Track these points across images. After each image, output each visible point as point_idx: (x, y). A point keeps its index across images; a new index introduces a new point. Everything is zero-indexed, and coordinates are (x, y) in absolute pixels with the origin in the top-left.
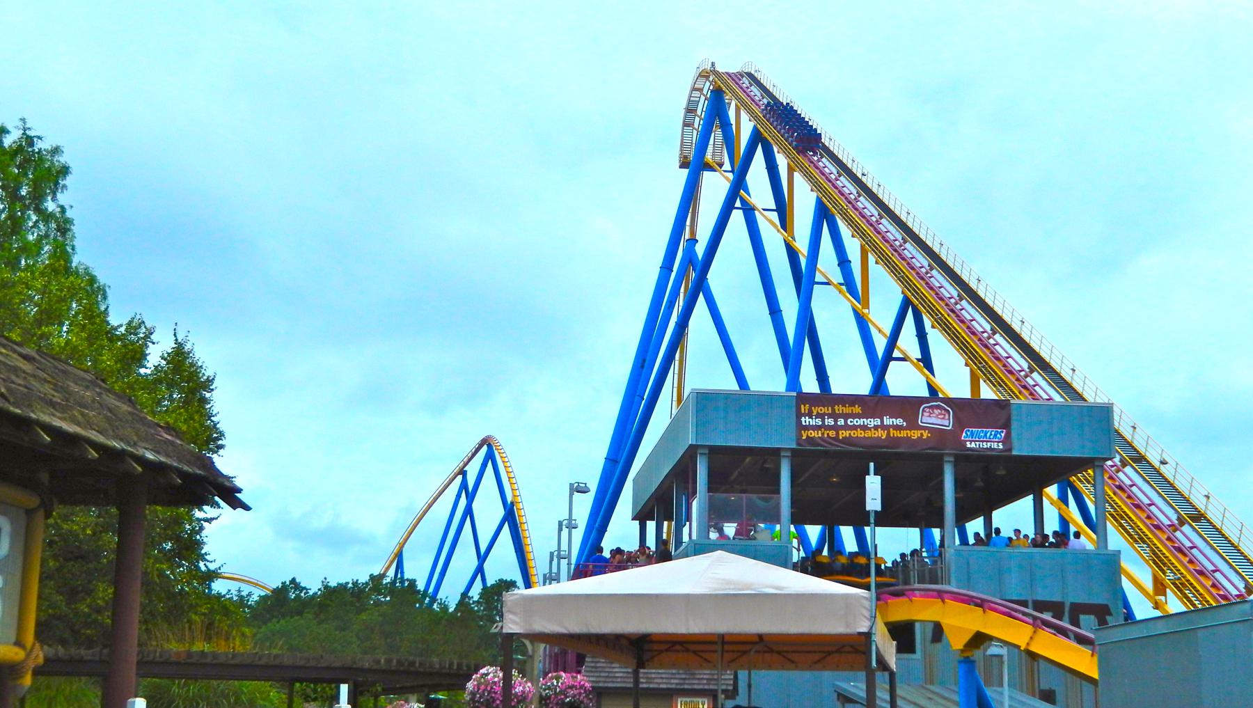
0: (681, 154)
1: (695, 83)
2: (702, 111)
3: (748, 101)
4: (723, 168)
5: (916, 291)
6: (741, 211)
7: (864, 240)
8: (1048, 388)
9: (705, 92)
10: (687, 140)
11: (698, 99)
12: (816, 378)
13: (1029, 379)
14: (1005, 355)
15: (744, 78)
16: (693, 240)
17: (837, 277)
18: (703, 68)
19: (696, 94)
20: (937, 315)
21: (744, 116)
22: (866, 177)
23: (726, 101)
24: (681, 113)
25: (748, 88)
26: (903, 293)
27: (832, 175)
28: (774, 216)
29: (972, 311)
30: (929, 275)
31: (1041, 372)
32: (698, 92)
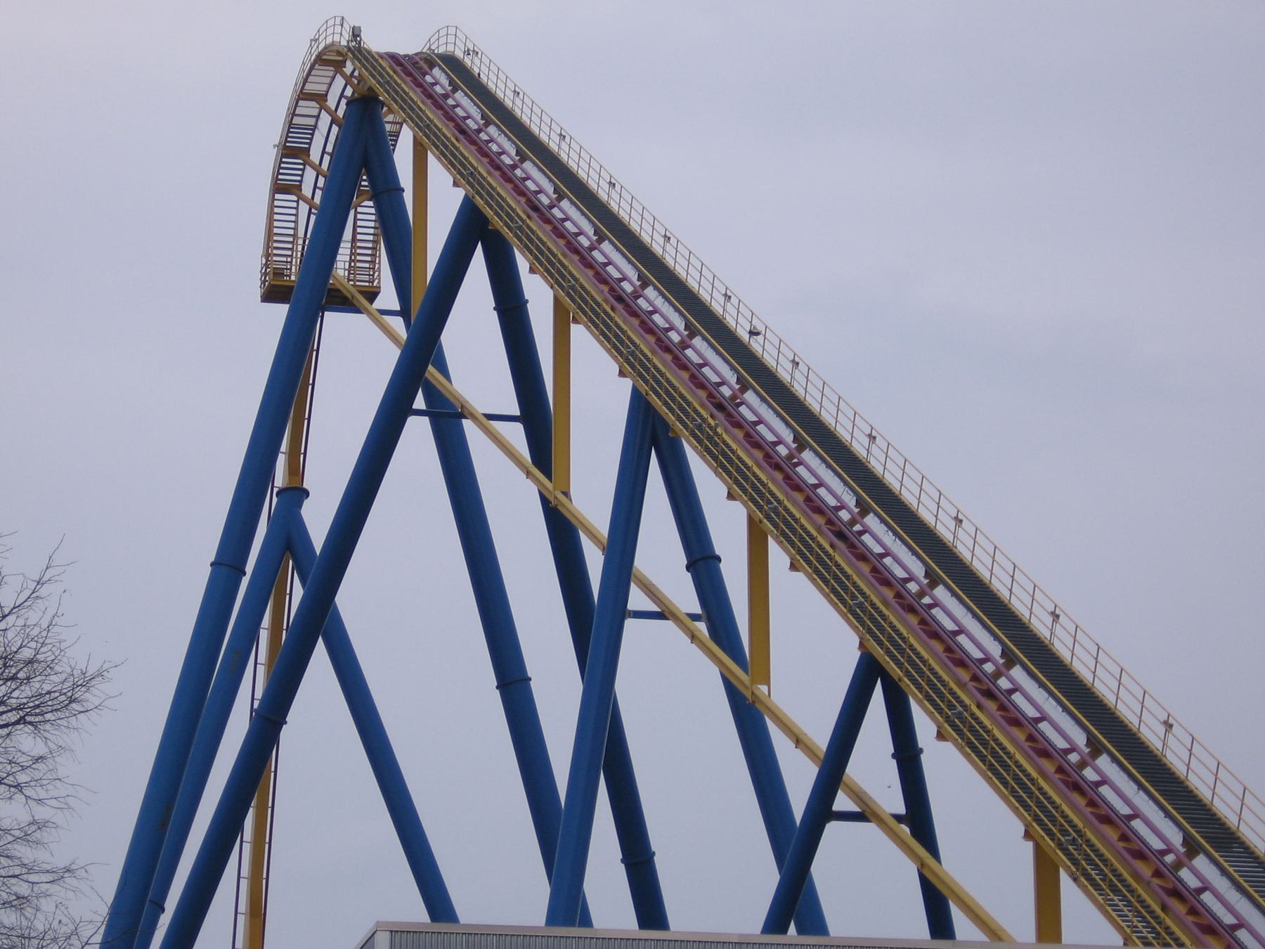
0: (267, 266)
1: (305, 81)
2: (324, 152)
3: (598, 293)
4: (379, 303)
5: (897, 645)
6: (426, 420)
7: (760, 508)
8: (1233, 896)
9: (331, 102)
10: (283, 227)
11: (311, 121)
12: (620, 856)
13: (596, 254)
14: (1125, 810)
15: (436, 71)
16: (296, 494)
17: (686, 598)
18: (329, 40)
19: (309, 107)
20: (951, 707)
21: (437, 173)
22: (760, 338)
23: (388, 127)
24: (270, 156)
25: (446, 96)
26: (862, 645)
27: (582, 239)
28: (516, 434)
29: (1039, 695)
30: (857, 528)
31: (1216, 855)
32: (314, 104)
